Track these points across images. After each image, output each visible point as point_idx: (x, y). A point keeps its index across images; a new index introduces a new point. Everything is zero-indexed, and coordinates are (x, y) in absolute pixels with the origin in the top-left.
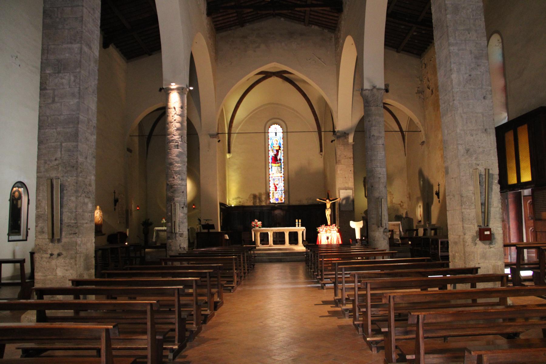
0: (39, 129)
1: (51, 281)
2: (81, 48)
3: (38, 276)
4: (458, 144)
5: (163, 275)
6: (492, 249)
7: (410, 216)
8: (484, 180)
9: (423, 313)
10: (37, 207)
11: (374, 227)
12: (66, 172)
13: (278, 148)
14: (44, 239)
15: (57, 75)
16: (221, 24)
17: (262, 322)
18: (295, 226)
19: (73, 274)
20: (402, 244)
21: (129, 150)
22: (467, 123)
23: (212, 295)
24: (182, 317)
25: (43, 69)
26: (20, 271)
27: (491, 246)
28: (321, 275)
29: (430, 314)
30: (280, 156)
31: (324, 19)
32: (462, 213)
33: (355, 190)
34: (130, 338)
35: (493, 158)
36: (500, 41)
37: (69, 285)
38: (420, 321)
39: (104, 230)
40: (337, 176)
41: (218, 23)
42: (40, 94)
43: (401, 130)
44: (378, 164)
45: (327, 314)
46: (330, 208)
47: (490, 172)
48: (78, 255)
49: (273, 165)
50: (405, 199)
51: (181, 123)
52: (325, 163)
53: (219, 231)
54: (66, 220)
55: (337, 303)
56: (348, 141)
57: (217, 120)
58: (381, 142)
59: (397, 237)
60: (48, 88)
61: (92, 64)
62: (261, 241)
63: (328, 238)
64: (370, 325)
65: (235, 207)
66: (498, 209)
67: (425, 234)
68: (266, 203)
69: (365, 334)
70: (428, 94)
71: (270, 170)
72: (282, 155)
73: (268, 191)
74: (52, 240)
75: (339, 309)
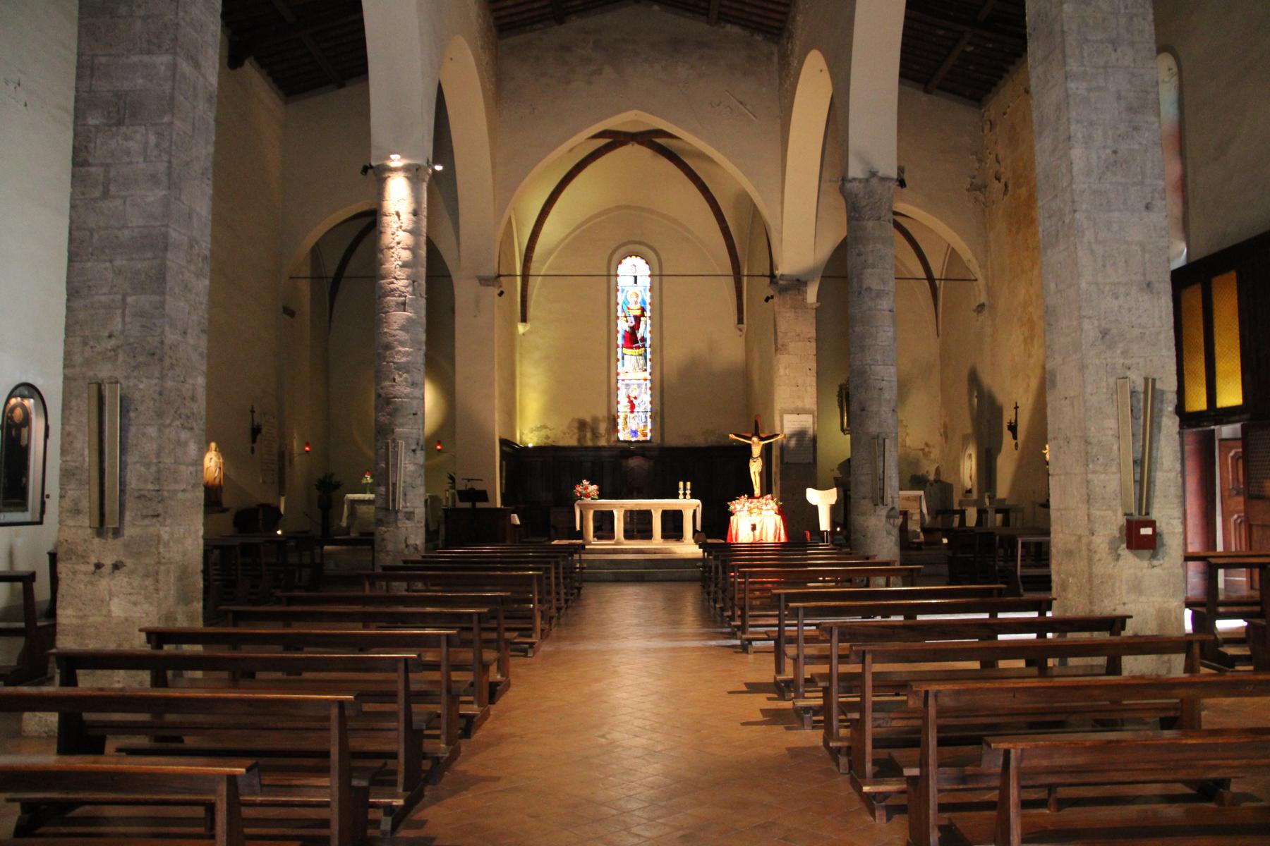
0: (70, 261)
1: (96, 628)
2: (174, 67)
3: (66, 616)
4: (1080, 317)
5: (367, 619)
6: (1156, 570)
7: (945, 477)
8: (1144, 403)
9: (1021, 746)
10: (64, 451)
11: (866, 504)
12: (135, 367)
13: (638, 313)
14: (81, 527)
15: (114, 129)
16: (511, 15)
17: (603, 736)
18: (676, 496)
19: (149, 615)
20: (926, 543)
21: (289, 312)
22: (1104, 266)
23: (485, 667)
24: (414, 727)
25: (79, 114)
26: (22, 596)
27: (1155, 562)
28: (742, 617)
29: (1037, 747)
30: (644, 330)
31: (755, 11)
32: (1088, 482)
33: (819, 416)
34: (287, 783)
35: (1164, 352)
36: (1175, 70)
37: (139, 643)
38: (1013, 763)
39: (227, 500)
40: (777, 381)
41: (503, 13)
42: (73, 176)
43: (930, 278)
44: (879, 357)
45: (760, 717)
46: (761, 456)
47: (1158, 386)
48: (162, 568)
49: (626, 351)
50: (936, 439)
51: (413, 249)
52: (748, 351)
53: (499, 505)
54: (133, 483)
55: (781, 689)
56: (804, 299)
57: (498, 244)
58: (885, 304)
59: (914, 526)
60: (91, 161)
61: (202, 105)
62: (596, 529)
63: (754, 528)
64: (869, 755)
65: (535, 448)
66: (1174, 474)
67: (980, 522)
68: (608, 440)
69: (857, 781)
70: (1008, 199)
71: (620, 364)
72: (649, 328)
73: (613, 412)
74: (101, 530)
75: (787, 705)
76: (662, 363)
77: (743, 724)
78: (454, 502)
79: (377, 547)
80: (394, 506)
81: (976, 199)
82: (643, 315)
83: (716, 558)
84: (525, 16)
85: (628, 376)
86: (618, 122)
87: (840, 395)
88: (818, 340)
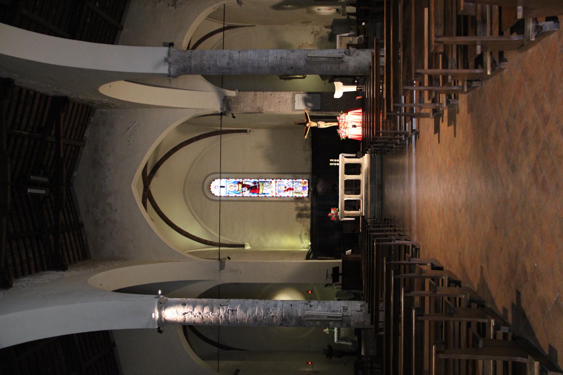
7: (330, 23)
11: (342, 67)
13: (240, 185)
16: (78, 252)
17: (460, 211)
20: (365, 33)
30: (250, 182)
33: (295, 90)
40: (277, 113)
41: (76, 257)
44: (264, 59)
45: (452, 127)
46: (316, 122)
50: (309, 28)
51: (203, 306)
53: (341, 261)
55: (437, 114)
56: (234, 97)
58: (236, 55)
63: (354, 126)
65: (311, 241)
68: (308, 202)
71: (267, 196)
72: (249, 180)
73: (292, 199)
76: (267, 173)
77: (455, 136)
78: (339, 285)
79: (362, 327)
80: (340, 317)
81: (181, 4)
82: (242, 183)
83: (369, 147)
84: (78, 244)
85: (274, 191)
86: (138, 196)
87: (285, 79)
88: (255, 91)
